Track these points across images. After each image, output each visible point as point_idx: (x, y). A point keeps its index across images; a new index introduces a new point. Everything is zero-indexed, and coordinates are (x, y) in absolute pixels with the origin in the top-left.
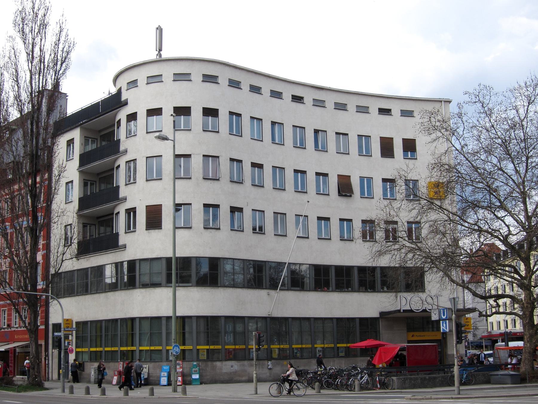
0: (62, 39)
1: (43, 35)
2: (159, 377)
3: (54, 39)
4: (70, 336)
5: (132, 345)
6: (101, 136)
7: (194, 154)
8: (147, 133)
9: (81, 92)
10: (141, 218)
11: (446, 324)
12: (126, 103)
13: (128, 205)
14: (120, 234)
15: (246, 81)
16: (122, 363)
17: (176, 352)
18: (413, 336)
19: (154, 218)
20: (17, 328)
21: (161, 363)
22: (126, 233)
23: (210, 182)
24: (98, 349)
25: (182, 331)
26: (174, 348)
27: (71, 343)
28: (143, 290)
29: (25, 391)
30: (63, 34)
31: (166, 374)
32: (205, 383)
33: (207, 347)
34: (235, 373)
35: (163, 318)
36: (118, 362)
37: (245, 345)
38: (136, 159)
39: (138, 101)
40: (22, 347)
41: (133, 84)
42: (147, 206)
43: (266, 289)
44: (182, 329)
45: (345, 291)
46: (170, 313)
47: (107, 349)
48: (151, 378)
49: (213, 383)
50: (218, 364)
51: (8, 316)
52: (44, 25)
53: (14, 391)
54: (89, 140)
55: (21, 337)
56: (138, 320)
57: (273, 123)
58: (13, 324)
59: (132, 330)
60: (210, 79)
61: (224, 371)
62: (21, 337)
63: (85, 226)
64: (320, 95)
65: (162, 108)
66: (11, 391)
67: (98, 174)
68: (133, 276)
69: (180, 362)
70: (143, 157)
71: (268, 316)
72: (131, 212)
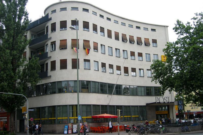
5: (54, 117)
7: (80, 39)
10: (58, 65)
11: (181, 106)
12: (51, 19)
14: (152, 43)
15: (106, 16)
18: (158, 113)
19: (64, 65)
31: (66, 129)
35: (68, 106)
41: (54, 11)
45: (126, 95)
46: (76, 103)
59: (54, 111)
64: (124, 21)
71: (107, 105)
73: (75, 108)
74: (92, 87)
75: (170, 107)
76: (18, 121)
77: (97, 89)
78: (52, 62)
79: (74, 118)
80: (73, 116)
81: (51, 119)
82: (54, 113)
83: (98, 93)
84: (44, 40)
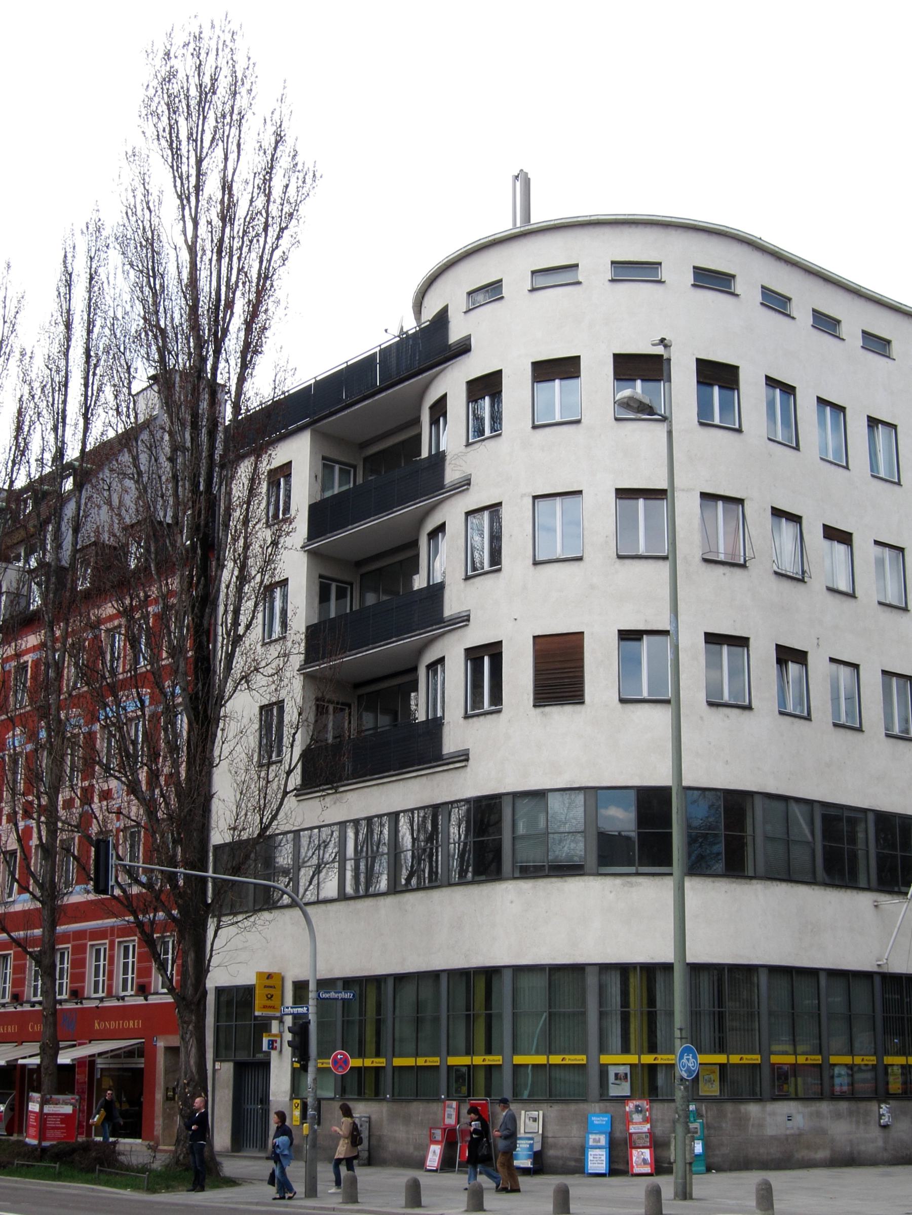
0: (284, 162)
1: (233, 148)
2: (583, 1150)
3: (261, 162)
4: (275, 1025)
5: (489, 1051)
6: (366, 460)
8: (535, 427)
9: (312, 334)
13: (475, 636)
14: (445, 721)
15: (806, 297)
16: (454, 1104)
17: (689, 1071)
20: (101, 1000)
21: (582, 1106)
22: (467, 717)
23: (721, 570)
24: (368, 1062)
25: (645, 1009)
26: (681, 1057)
27: (278, 1045)
28: (526, 886)
29: (169, 1188)
30: (284, 151)
31: (603, 1140)
32: (719, 1169)
33: (721, 1059)
34: (798, 1137)
35: (588, 969)
36: (439, 1100)
37: (820, 1053)
38: (500, 504)
39: (502, 341)
40: (114, 1054)
42: (535, 637)
43: (869, 889)
44: (645, 1001)
46: (664, 953)
47: (398, 1062)
48: (551, 1152)
49: (731, 1169)
50: (753, 1109)
51: (73, 966)
52: (234, 118)
53: (136, 1187)
54: (332, 468)
55: (113, 1025)
56: (507, 977)
57: (873, 423)
58: (89, 990)
60: (711, 279)
61: (770, 1131)
62: (113, 1025)
63: (321, 709)
65: (578, 358)
66: (125, 1186)
67: (358, 564)
68: (490, 842)
69: (645, 1104)
70: (523, 496)
71: (876, 969)
72: (486, 658)
73: (635, 981)
74: (767, 838)
75: (493, 1018)
76: (226, 1070)
77: (800, 855)
78: (474, 655)
79: (633, 1059)
80: (626, 1050)
81: (465, 1060)
82: (489, 1019)
83: (812, 881)
84: (403, 500)
